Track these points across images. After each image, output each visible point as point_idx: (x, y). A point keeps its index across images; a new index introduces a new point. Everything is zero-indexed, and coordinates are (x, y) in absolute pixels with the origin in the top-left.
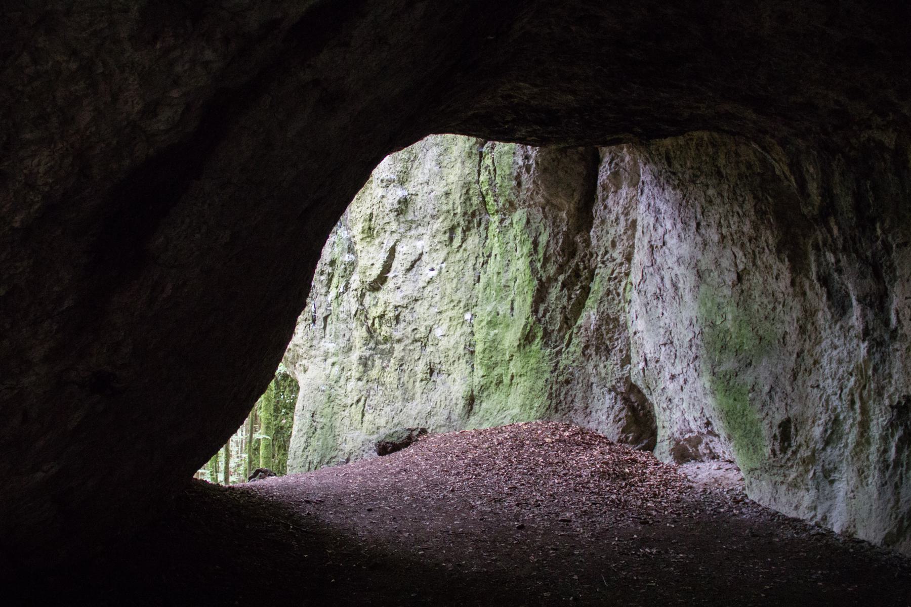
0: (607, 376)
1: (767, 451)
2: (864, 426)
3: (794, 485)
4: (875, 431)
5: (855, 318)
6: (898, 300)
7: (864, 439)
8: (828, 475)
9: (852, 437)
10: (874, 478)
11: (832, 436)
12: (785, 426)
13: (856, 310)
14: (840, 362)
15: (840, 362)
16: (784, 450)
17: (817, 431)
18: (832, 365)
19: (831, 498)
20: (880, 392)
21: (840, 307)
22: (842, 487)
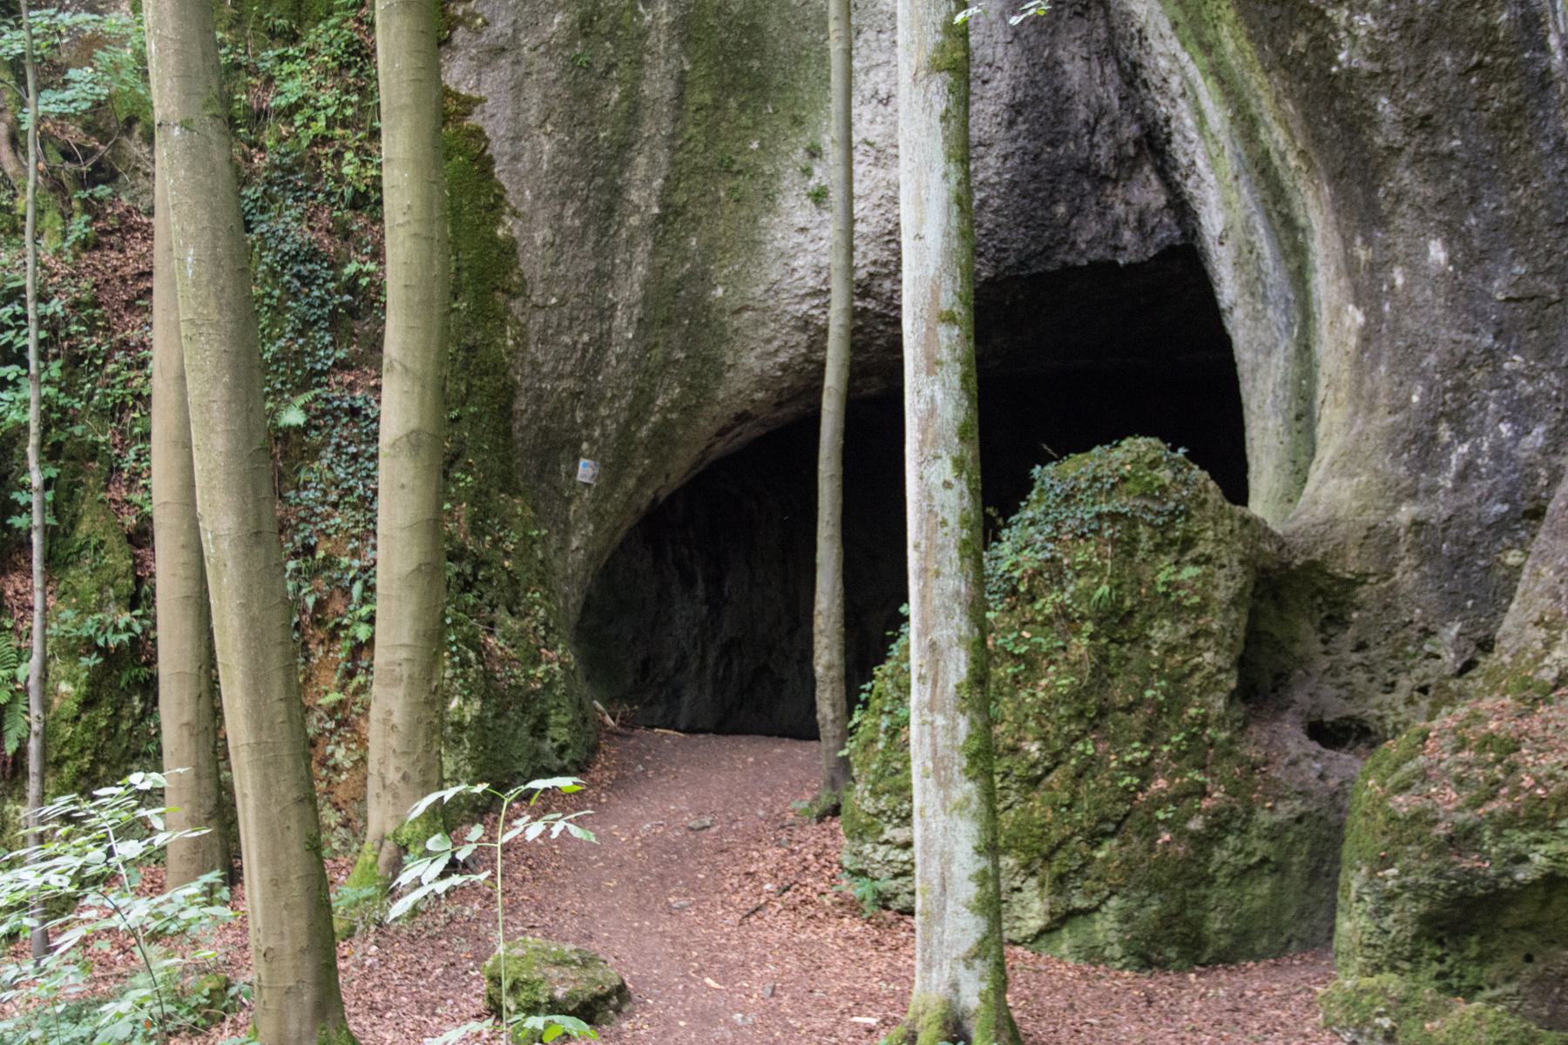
0: (191, 968)
1: (630, 681)
2: (703, 658)
3: (651, 704)
4: (710, 661)
5: (700, 590)
6: (888, 828)
7: (702, 668)
8: (677, 693)
9: (694, 667)
10: (708, 690)
11: (681, 665)
12: (645, 663)
13: (701, 585)
14: (688, 619)
15: (688, 619)
16: (643, 679)
17: (671, 664)
18: (708, 823)
19: (709, 1021)
20: (714, 636)
21: (689, 582)
22: (686, 699)
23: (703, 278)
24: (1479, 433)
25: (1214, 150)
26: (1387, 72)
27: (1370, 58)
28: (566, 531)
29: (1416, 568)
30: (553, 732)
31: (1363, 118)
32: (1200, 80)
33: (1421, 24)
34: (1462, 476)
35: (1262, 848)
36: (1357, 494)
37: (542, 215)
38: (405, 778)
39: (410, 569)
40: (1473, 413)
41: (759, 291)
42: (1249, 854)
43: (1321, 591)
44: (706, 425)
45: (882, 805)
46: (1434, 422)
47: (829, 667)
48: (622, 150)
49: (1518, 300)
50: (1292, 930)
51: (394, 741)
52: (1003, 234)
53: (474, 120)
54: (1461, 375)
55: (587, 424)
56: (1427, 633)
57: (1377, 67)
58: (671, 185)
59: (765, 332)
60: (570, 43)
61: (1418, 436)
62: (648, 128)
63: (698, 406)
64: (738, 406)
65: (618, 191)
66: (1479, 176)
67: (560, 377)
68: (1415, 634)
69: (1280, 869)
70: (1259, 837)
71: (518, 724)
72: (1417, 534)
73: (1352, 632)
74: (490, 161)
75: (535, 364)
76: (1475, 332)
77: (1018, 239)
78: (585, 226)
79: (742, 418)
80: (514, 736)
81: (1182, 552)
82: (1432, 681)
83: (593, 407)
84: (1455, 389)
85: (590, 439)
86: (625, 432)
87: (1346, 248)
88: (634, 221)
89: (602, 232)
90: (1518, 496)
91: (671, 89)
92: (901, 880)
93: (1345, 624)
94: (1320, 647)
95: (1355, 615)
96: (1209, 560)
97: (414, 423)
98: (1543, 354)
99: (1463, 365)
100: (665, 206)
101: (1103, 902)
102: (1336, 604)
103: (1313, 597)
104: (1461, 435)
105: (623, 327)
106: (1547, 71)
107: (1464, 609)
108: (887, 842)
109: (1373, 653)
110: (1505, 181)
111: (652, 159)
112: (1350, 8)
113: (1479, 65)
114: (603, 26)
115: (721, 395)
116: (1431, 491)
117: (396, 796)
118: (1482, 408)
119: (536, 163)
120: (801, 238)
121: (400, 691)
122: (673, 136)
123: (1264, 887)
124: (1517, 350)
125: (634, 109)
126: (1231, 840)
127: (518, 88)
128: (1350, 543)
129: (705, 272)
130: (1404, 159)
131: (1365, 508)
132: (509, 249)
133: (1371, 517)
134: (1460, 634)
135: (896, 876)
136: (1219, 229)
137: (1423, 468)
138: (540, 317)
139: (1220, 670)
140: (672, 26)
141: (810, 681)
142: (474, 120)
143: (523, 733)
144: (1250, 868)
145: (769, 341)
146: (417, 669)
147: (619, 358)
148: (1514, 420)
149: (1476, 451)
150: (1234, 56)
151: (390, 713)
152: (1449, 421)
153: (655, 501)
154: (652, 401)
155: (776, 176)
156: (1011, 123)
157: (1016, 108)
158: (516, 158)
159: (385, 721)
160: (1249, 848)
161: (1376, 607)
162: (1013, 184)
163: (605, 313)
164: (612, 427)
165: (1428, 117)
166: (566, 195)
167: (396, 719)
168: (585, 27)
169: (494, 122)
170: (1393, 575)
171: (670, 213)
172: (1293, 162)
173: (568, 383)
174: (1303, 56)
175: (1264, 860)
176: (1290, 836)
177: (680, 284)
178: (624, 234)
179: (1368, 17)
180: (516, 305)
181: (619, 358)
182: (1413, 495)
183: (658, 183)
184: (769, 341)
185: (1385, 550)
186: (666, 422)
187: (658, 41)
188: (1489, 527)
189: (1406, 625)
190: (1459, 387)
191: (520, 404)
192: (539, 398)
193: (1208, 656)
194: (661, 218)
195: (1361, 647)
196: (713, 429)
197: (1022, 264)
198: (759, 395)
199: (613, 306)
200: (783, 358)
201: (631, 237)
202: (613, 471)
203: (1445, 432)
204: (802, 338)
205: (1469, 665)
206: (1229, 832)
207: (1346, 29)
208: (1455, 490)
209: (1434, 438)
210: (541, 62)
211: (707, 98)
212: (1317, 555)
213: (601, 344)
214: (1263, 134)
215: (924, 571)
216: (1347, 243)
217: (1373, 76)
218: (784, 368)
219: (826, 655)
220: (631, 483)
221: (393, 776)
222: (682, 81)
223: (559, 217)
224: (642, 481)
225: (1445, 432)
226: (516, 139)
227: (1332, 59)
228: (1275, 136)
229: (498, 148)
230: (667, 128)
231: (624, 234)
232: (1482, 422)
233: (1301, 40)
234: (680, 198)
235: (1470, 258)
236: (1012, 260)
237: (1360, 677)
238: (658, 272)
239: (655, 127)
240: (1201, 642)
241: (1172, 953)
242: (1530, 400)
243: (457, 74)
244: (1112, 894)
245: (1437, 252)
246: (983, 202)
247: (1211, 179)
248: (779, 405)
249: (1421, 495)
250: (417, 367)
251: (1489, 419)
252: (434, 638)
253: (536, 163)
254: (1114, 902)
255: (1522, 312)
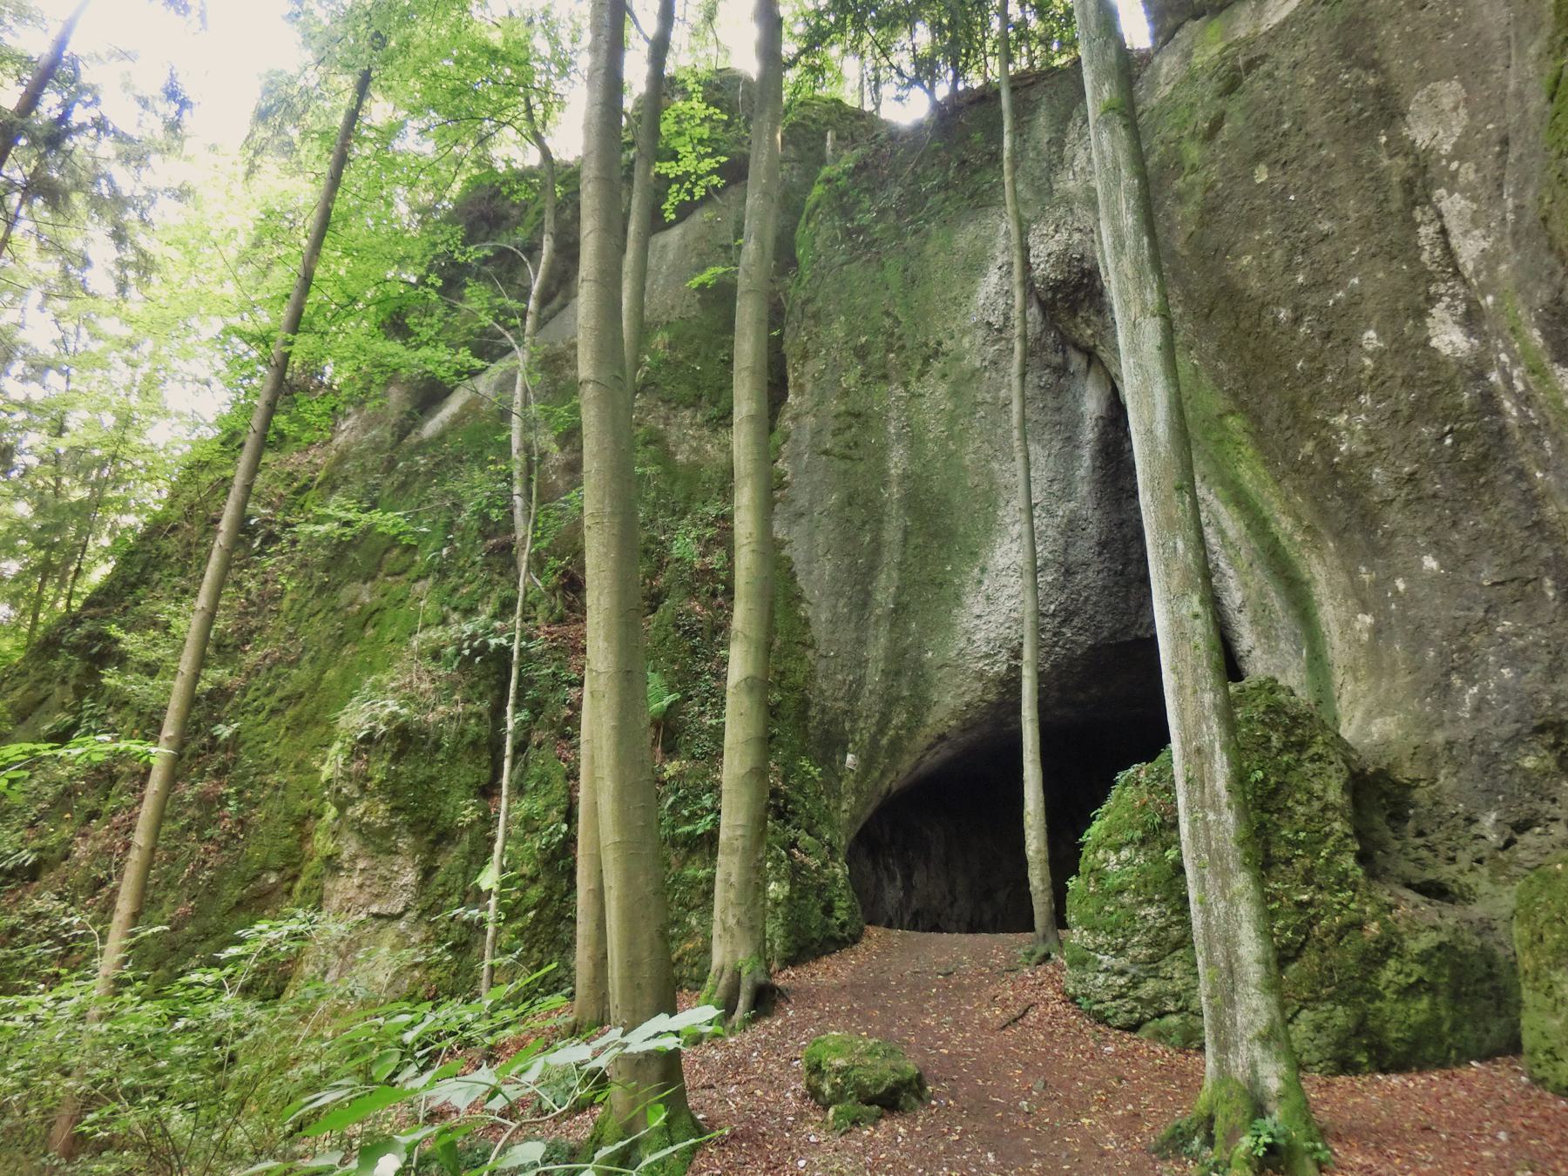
5: (899, 883)
23: (920, 648)
24: (1486, 675)
25: (1231, 552)
26: (1380, 450)
27: (1366, 443)
28: (840, 797)
29: (1455, 774)
30: (838, 913)
31: (1361, 486)
32: (1222, 509)
33: (1406, 412)
34: (1477, 709)
35: (1418, 971)
36: (1400, 726)
37: (825, 605)
38: (738, 922)
39: (743, 772)
40: (1477, 666)
41: (953, 654)
42: (1409, 975)
43: (1386, 795)
44: (921, 741)
45: (1100, 940)
46: (1447, 674)
47: (1038, 852)
48: (872, 569)
49: (1502, 583)
50: (1450, 1040)
51: (732, 895)
52: (1099, 617)
53: (785, 553)
54: (1462, 640)
55: (852, 731)
56: (1471, 821)
57: (1371, 449)
58: (901, 590)
59: (957, 680)
60: (842, 509)
61: (1436, 685)
62: (886, 557)
63: (917, 727)
64: (941, 729)
65: (869, 594)
66: (1457, 506)
67: (836, 700)
68: (1462, 822)
69: (1432, 989)
70: (1413, 961)
71: (814, 905)
72: (1450, 750)
73: (1411, 825)
74: (794, 575)
75: (822, 692)
76: (1469, 609)
77: (1108, 624)
78: (851, 612)
79: (942, 738)
80: (811, 912)
81: (1300, 752)
82: (1485, 854)
83: (854, 721)
84: (1460, 650)
85: (853, 740)
86: (874, 740)
87: (1351, 579)
88: (878, 611)
89: (861, 617)
90: (1528, 716)
91: (899, 536)
92: (1118, 1002)
93: (1406, 819)
94: (1390, 834)
95: (1411, 812)
96: (1320, 758)
97: (750, 671)
98: (1529, 616)
99: (1464, 632)
100: (897, 604)
101: (1295, 1015)
102: (1395, 804)
103: (1379, 798)
104: (1471, 682)
105: (874, 677)
106: (1503, 428)
107: (1497, 801)
108: (1106, 970)
109: (1431, 838)
110: (1479, 506)
111: (889, 576)
112: (1349, 413)
113: (1451, 431)
114: (860, 501)
115: (930, 721)
116: (1455, 720)
117: (732, 936)
118: (1484, 661)
119: (821, 576)
120: (977, 622)
121: (736, 859)
122: (901, 563)
123: (1424, 1003)
124: (1506, 617)
125: (877, 547)
126: (1392, 963)
127: (811, 536)
128: (1404, 758)
129: (921, 642)
130: (1396, 505)
131: (1408, 735)
132: (807, 623)
133: (1415, 740)
134: (1498, 821)
135: (1114, 998)
136: (1238, 602)
137: (1444, 706)
138: (823, 662)
139: (1347, 836)
140: (899, 500)
141: (1023, 863)
142: (785, 553)
143: (818, 911)
144: (1411, 986)
145: (959, 687)
146: (748, 843)
147: (871, 692)
148: (1511, 665)
149: (1484, 690)
150: (1250, 481)
151: (730, 874)
152: (1459, 672)
153: (889, 790)
154: (890, 721)
155: (962, 585)
156: (1100, 554)
157: (1103, 545)
158: (810, 573)
159: (726, 881)
160: (1407, 970)
161: (1428, 803)
162: (1105, 587)
163: (862, 663)
164: (866, 736)
165: (1413, 474)
166: (839, 595)
167: (733, 879)
168: (850, 501)
169: (796, 553)
170: (1437, 780)
171: (900, 611)
172: (1298, 538)
173: (841, 704)
174: (1311, 457)
175: (1420, 981)
176: (1435, 961)
177: (905, 651)
178: (873, 619)
179: (1363, 416)
180: (810, 654)
181: (871, 692)
182: (1441, 725)
183: (892, 590)
184: (959, 687)
185: (1430, 763)
186: (898, 738)
187: (893, 510)
188: (1507, 741)
189: (1453, 816)
190: (1463, 649)
191: (813, 712)
192: (823, 710)
193: (1337, 825)
194: (895, 611)
195: (1420, 834)
196: (925, 744)
197: (1112, 636)
198: (952, 723)
199: (867, 661)
200: (967, 698)
201: (877, 622)
202: (868, 763)
203: (1456, 681)
204: (979, 685)
205: (1509, 843)
206: (1389, 957)
207: (1347, 429)
208: (1473, 718)
209: (1448, 686)
210: (825, 521)
211: (920, 541)
212: (1383, 765)
213: (860, 682)
214: (1274, 527)
215: (1180, 688)
216: (1352, 574)
217: (1369, 454)
218: (968, 705)
219: (1035, 842)
220: (876, 774)
221: (731, 921)
222: (907, 533)
223: (835, 606)
224: (883, 774)
225: (1456, 681)
226: (809, 562)
227: (1336, 452)
228: (1284, 525)
229: (799, 567)
230: (897, 558)
231: (873, 619)
232: (1485, 671)
233: (1309, 447)
234: (905, 598)
235: (1455, 562)
236: (1105, 634)
237: (1424, 853)
238: (893, 642)
239: (891, 556)
240: (1330, 814)
241: (1362, 1058)
242: (1524, 650)
243: (779, 531)
244: (1302, 1008)
245: (1430, 563)
246: (1087, 599)
247: (1231, 572)
248: (964, 731)
249: (1447, 724)
250: (752, 635)
251: (1491, 668)
252: (758, 834)
253: (821, 576)
254: (1304, 1014)
255: (1508, 591)
